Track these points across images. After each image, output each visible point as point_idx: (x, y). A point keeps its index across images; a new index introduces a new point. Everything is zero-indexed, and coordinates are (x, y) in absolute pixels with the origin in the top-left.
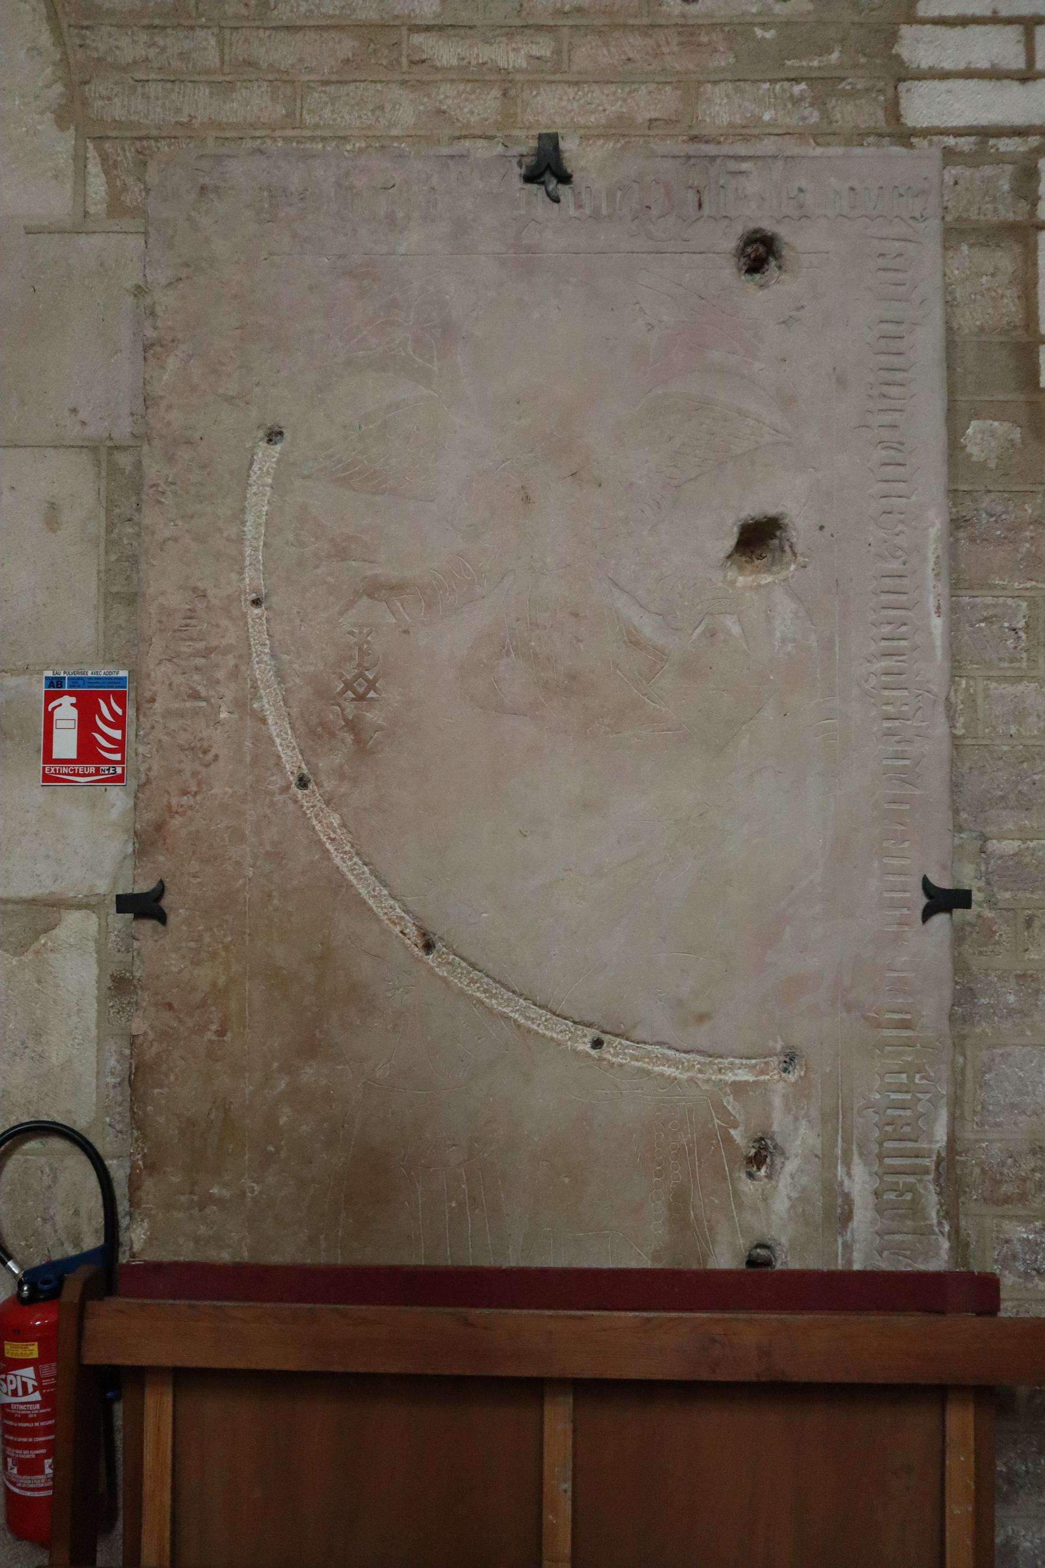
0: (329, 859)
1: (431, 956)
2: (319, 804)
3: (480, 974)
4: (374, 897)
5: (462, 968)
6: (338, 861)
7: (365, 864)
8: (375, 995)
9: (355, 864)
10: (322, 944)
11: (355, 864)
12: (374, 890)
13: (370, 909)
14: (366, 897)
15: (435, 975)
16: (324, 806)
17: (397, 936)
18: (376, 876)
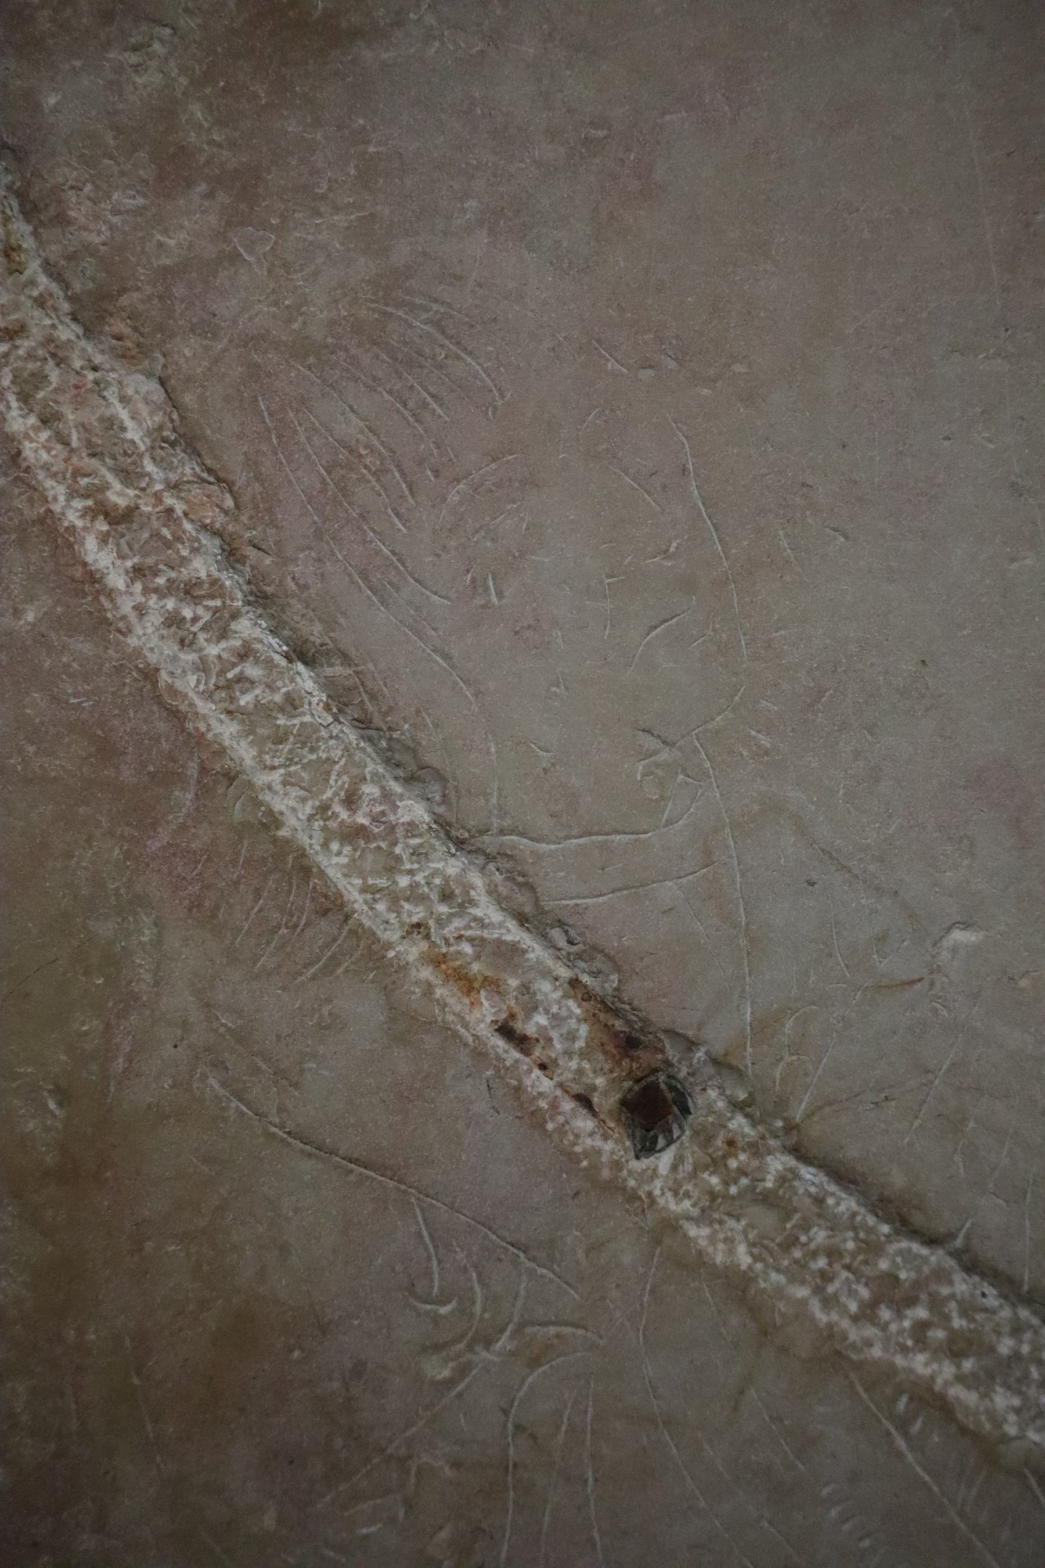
0: (103, 626)
1: (664, 1161)
2: (39, 323)
3: (936, 1257)
4: (354, 834)
5: (834, 1225)
6: (148, 638)
7: (302, 653)
8: (359, 1369)
9: (245, 654)
10: (63, 1095)
11: (245, 654)
12: (351, 801)
13: (332, 906)
14: (311, 841)
15: (696, 1264)
16: (67, 332)
17: (480, 1054)
18: (363, 723)
